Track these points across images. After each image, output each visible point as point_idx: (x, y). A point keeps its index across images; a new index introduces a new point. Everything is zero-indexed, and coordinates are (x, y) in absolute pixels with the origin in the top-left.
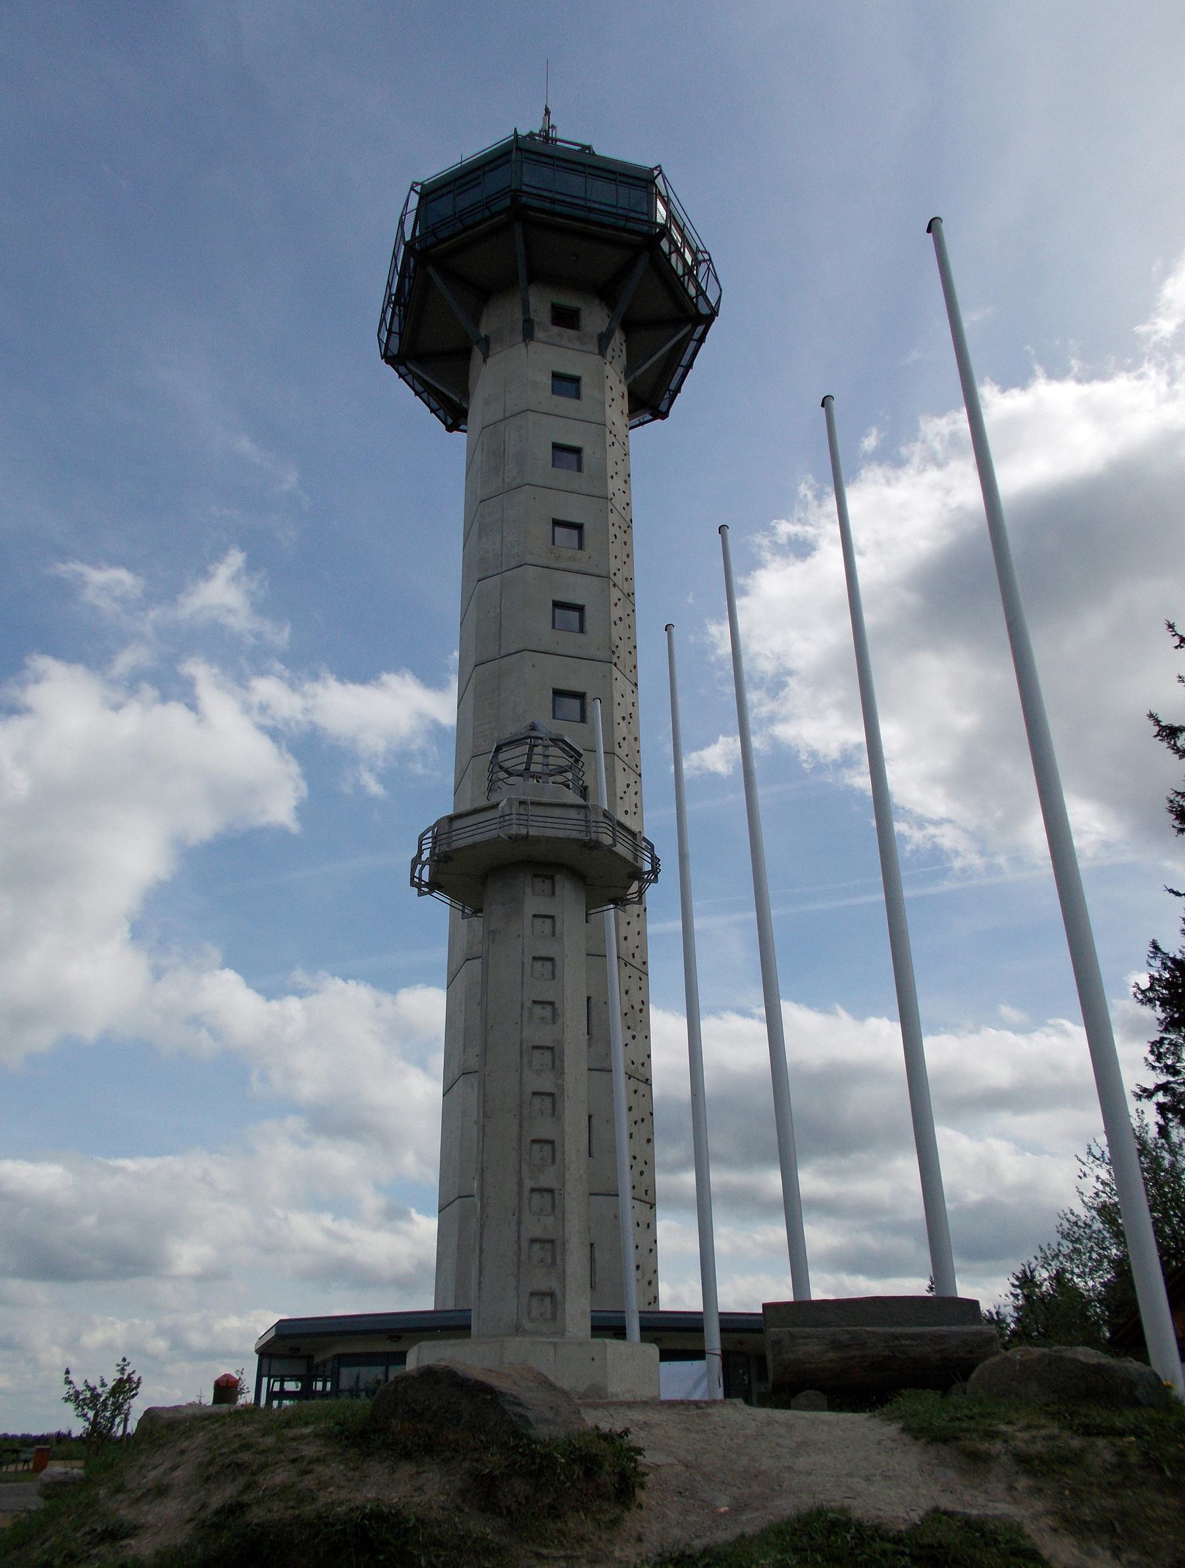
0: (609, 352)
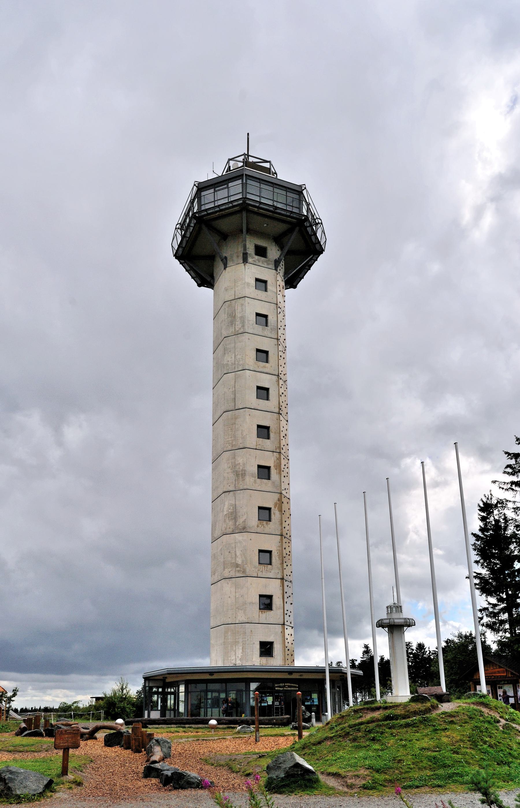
0: (278, 269)
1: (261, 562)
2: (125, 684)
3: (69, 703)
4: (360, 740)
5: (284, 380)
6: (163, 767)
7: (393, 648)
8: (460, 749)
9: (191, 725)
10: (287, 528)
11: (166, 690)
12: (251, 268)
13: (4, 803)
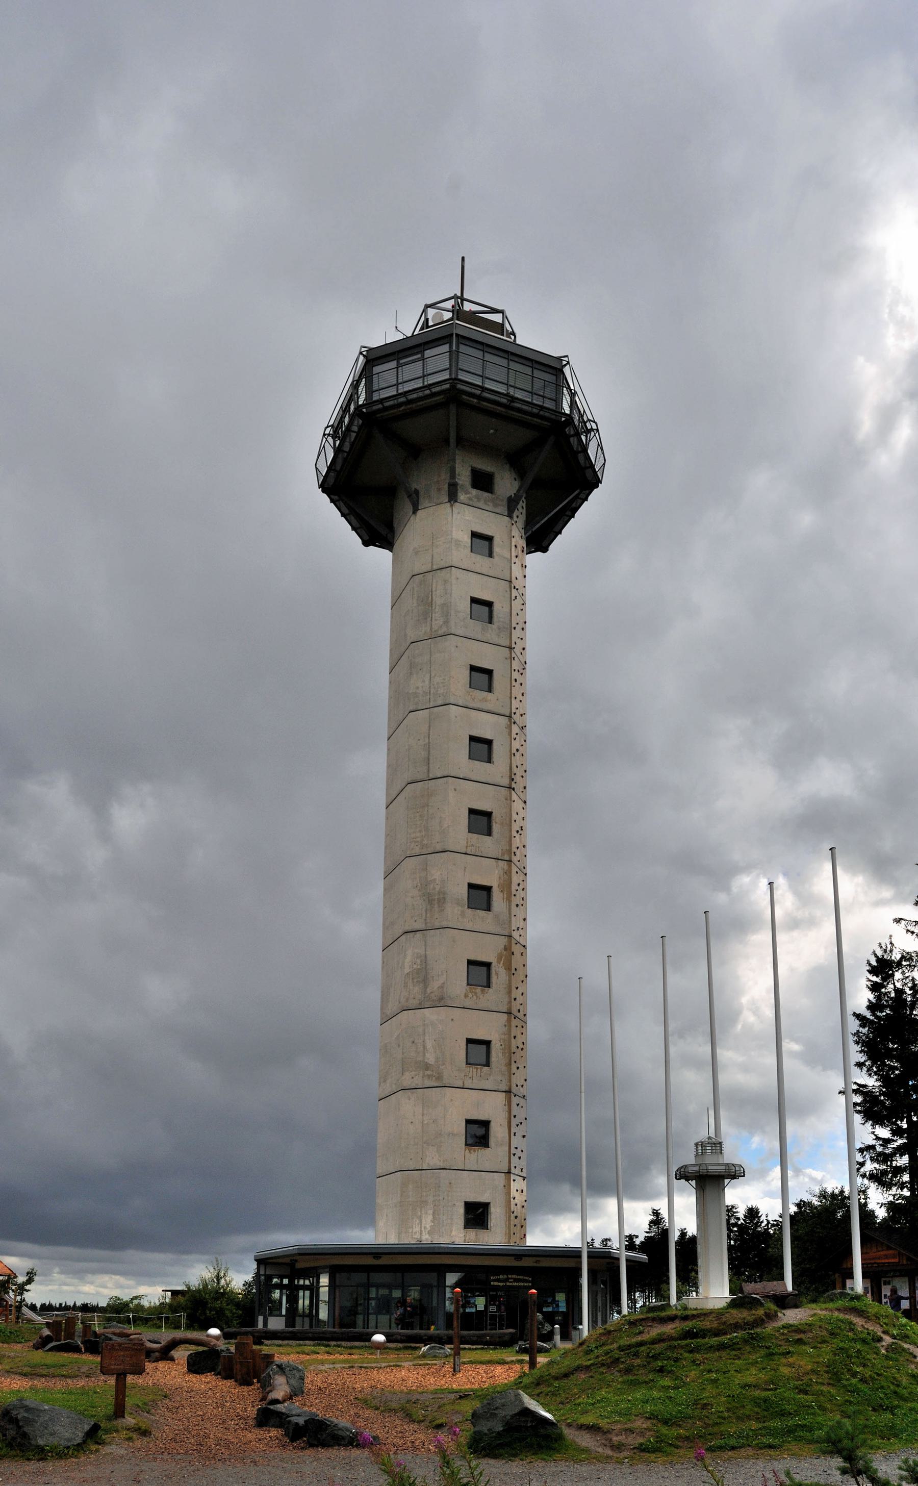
0: (516, 513)
3: (126, 1298)
4: (638, 1370)
6: (290, 1410)
7: (704, 1215)
8: (811, 1385)
9: (339, 1343)
10: (520, 999)
11: (296, 1281)
12: (464, 511)
13: (16, 1459)
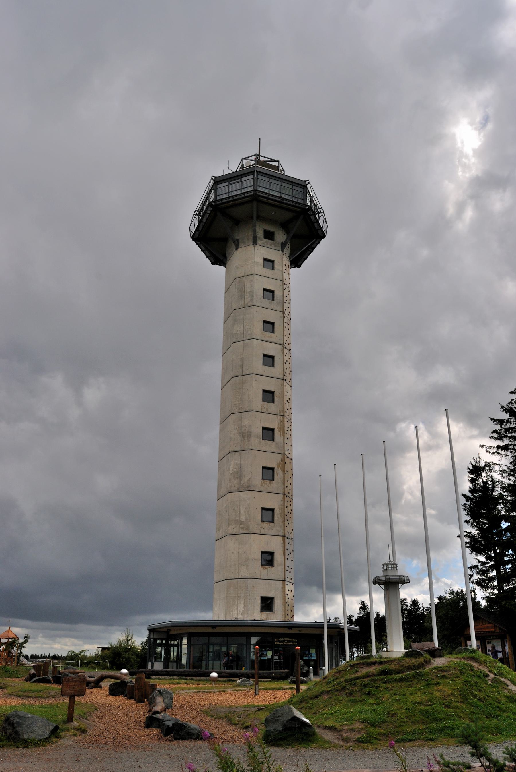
0: (285, 251)
1: (264, 520)
2: (130, 634)
3: (77, 651)
4: (356, 694)
5: (288, 349)
6: (164, 717)
8: (451, 702)
9: (192, 677)
11: (170, 642)
12: (260, 249)
13: (11, 747)
